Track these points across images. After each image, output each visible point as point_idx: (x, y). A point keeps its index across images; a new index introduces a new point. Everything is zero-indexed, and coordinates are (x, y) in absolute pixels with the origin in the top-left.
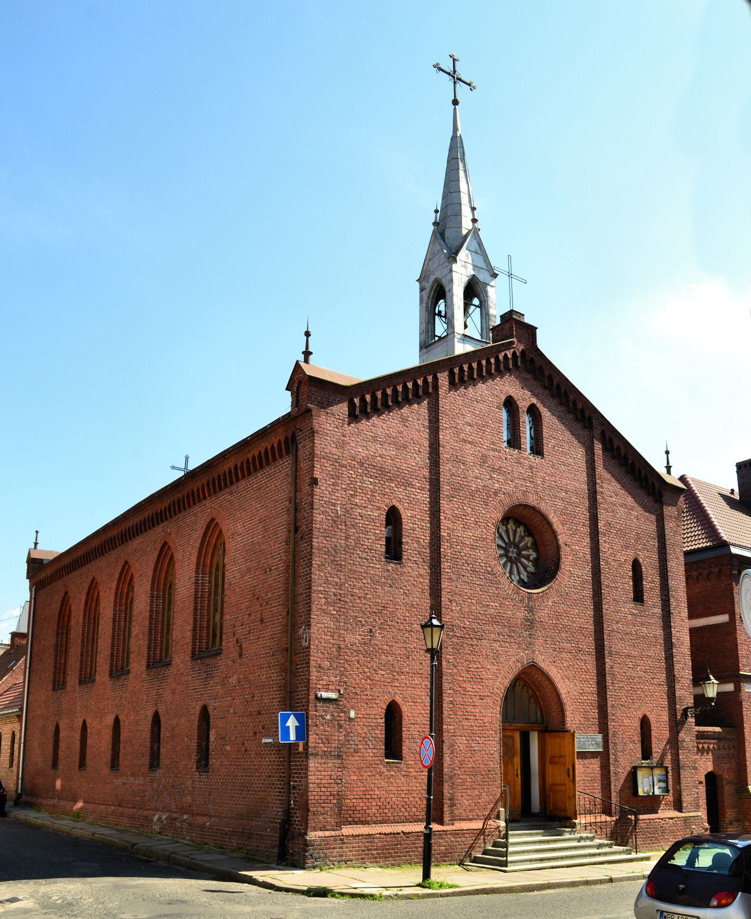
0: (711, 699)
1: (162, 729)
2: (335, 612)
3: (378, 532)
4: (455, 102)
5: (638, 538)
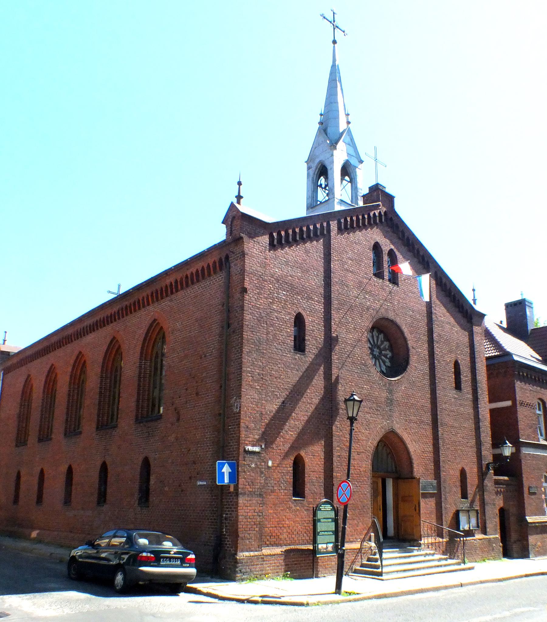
0: (507, 457)
1: (109, 475)
2: (259, 387)
3: (289, 330)
4: (334, 42)
5: (458, 347)
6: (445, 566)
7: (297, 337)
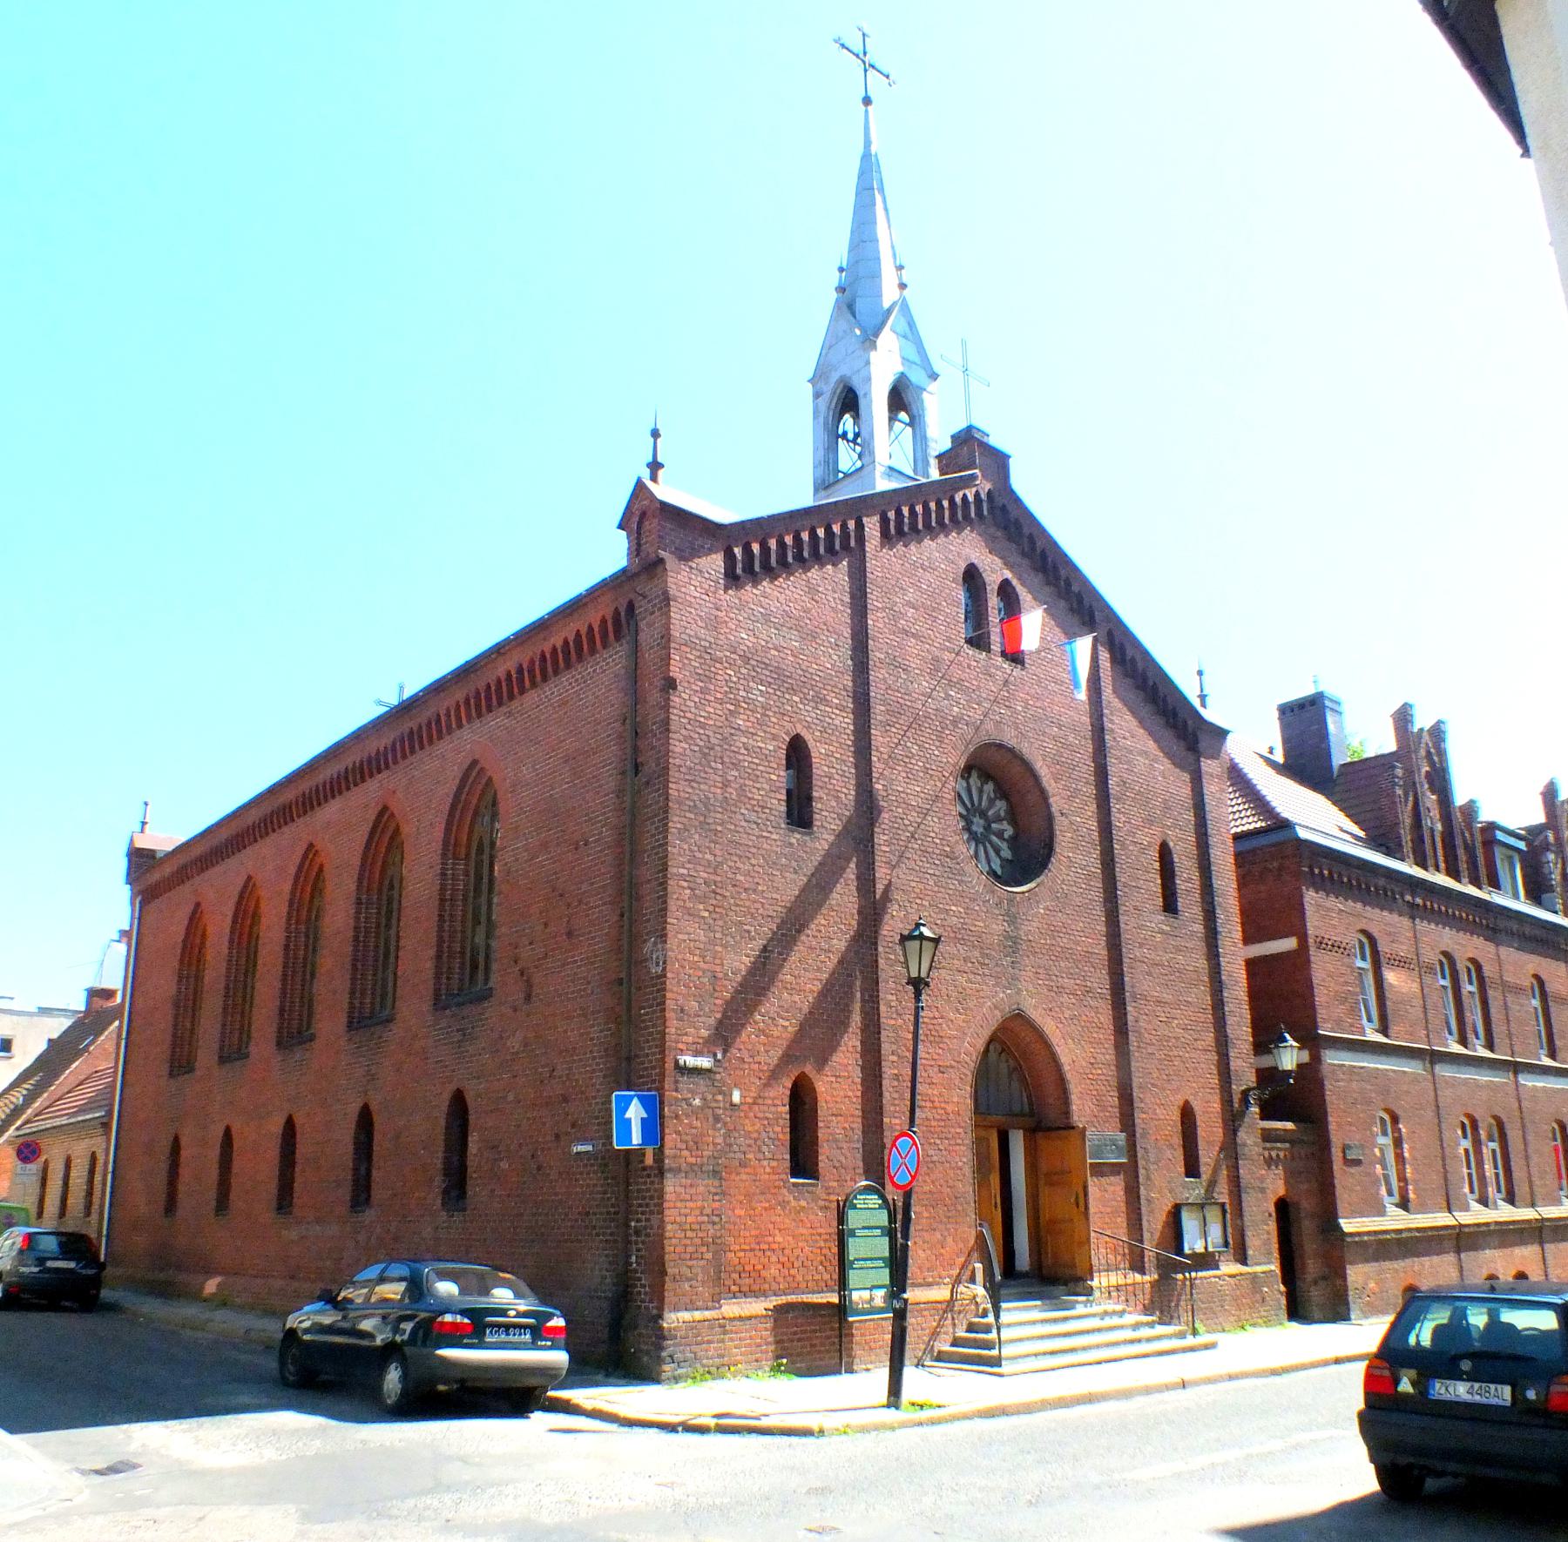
0: (1288, 1073)
2: (706, 914)
4: (867, 101)
5: (1167, 807)
6: (1149, 1340)
7: (795, 793)
